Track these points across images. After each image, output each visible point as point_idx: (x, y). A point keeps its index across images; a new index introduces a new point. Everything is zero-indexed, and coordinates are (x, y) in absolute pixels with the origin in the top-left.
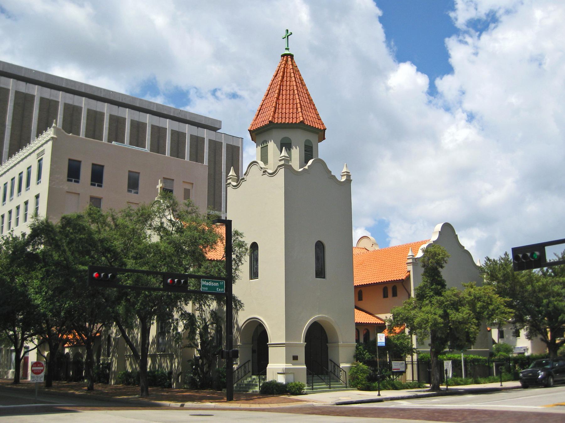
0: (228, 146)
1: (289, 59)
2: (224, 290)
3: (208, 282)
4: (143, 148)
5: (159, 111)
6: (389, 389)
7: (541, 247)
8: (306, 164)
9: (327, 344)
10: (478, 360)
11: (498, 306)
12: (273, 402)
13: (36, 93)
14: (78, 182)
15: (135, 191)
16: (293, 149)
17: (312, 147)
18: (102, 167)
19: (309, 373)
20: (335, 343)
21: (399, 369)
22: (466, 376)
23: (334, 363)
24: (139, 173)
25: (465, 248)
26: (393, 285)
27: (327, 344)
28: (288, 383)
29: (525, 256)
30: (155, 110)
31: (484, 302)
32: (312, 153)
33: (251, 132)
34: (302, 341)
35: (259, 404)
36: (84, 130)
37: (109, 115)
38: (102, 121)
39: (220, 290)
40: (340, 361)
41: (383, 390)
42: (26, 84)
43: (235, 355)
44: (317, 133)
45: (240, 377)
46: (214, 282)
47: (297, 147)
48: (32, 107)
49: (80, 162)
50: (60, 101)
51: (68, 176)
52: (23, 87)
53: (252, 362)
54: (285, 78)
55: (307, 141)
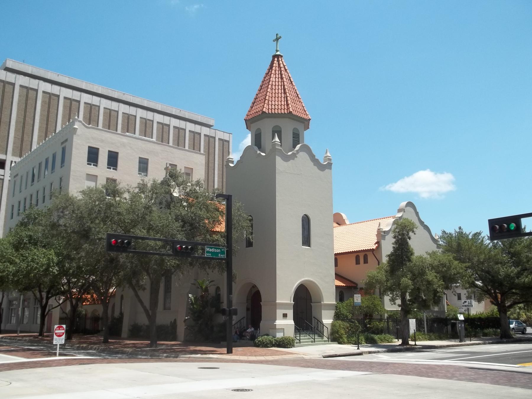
2: (225, 256)
3: (212, 248)
5: (163, 110)
8: (294, 149)
12: (267, 355)
17: (299, 134)
19: (296, 329)
26: (364, 253)
27: (311, 304)
29: (501, 227)
30: (160, 109)
32: (299, 139)
33: (247, 121)
35: (255, 356)
39: (221, 255)
42: (52, 85)
43: (235, 312)
44: (303, 123)
46: (216, 249)
51: (88, 161)
53: (247, 319)
55: (295, 129)
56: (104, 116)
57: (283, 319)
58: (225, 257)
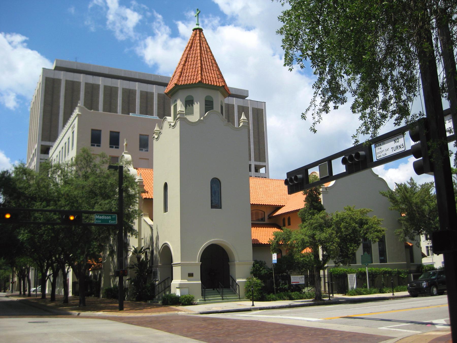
0: (254, 109)
1: (198, 32)
2: (116, 222)
3: (102, 216)
4: (152, 116)
6: (285, 300)
7: (305, 170)
9: (229, 263)
10: (390, 273)
11: (372, 226)
13: (100, 83)
14: (99, 146)
15: (146, 149)
16: (195, 104)
18: (118, 133)
20: (233, 262)
21: (299, 282)
22: (370, 287)
23: (233, 279)
24: (148, 136)
25: (379, 176)
28: (182, 295)
31: (346, 223)
34: (197, 261)
36: (139, 107)
37: (157, 94)
38: (152, 98)
40: (236, 277)
41: (279, 300)
45: (160, 290)
46: (107, 216)
47: (198, 102)
48: (98, 93)
49: (100, 131)
50: (119, 87)
52: (91, 79)
54: (192, 49)
56: (141, 98)
58: (116, 223)
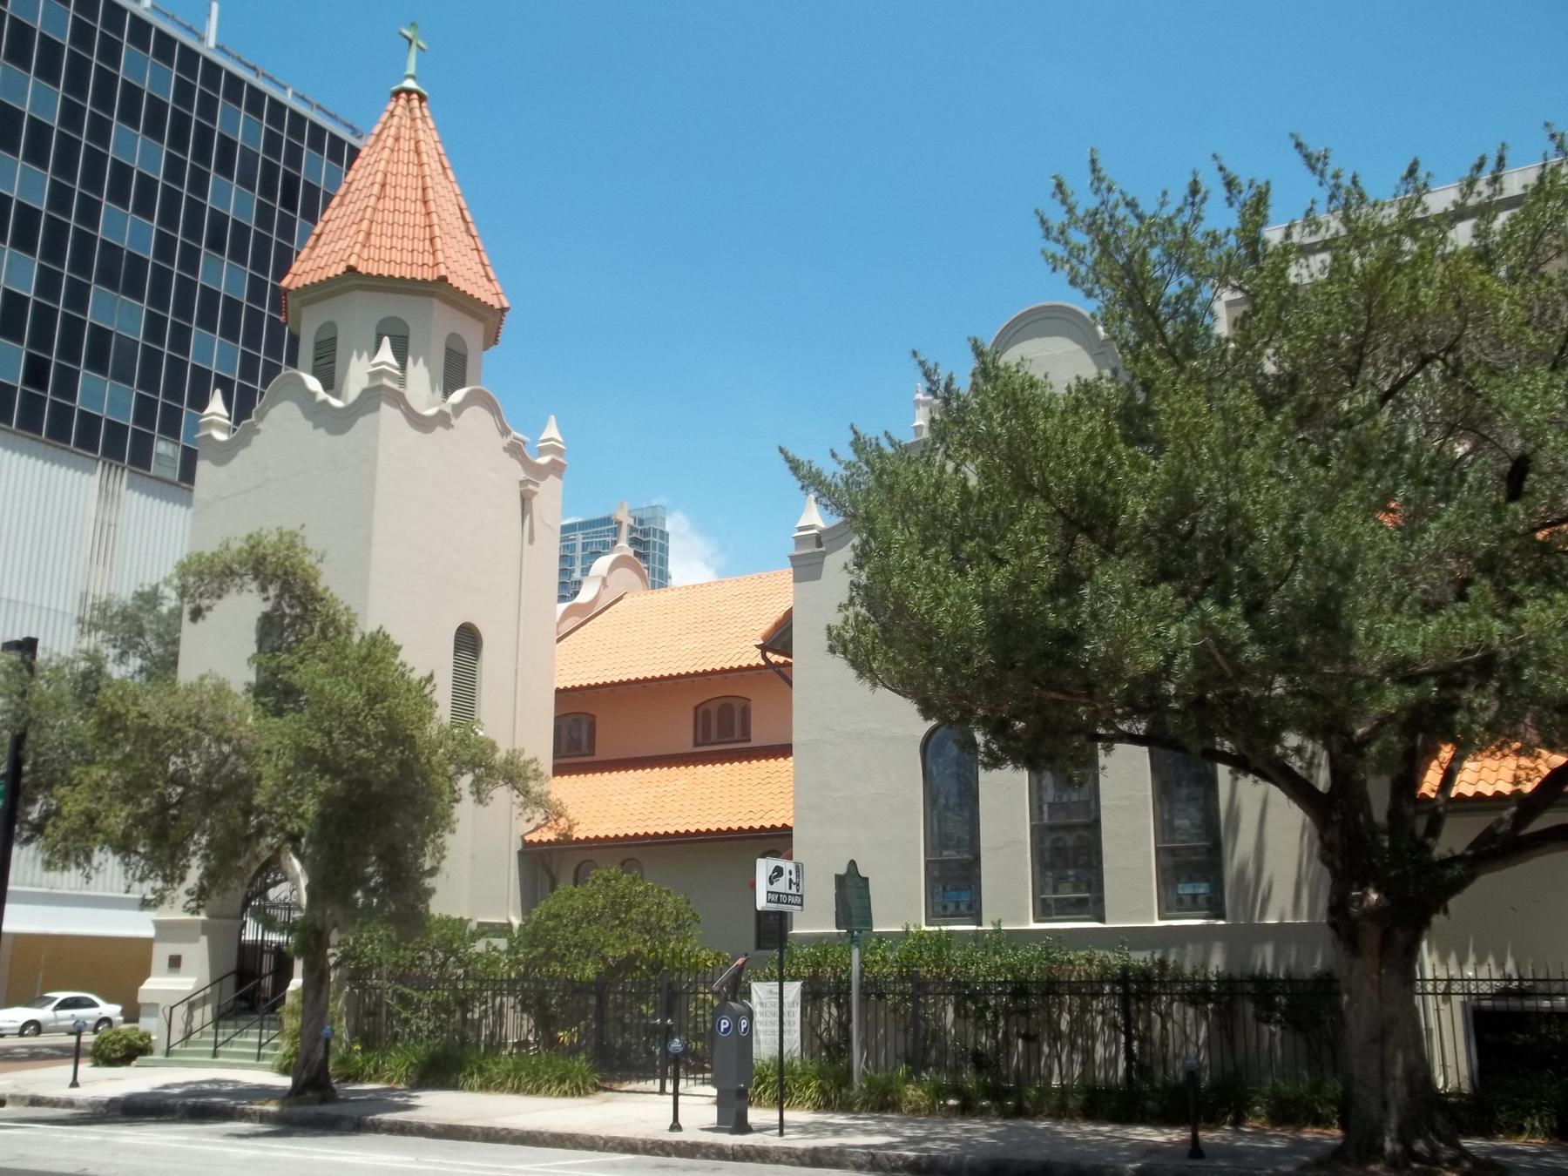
57: (169, 972)
